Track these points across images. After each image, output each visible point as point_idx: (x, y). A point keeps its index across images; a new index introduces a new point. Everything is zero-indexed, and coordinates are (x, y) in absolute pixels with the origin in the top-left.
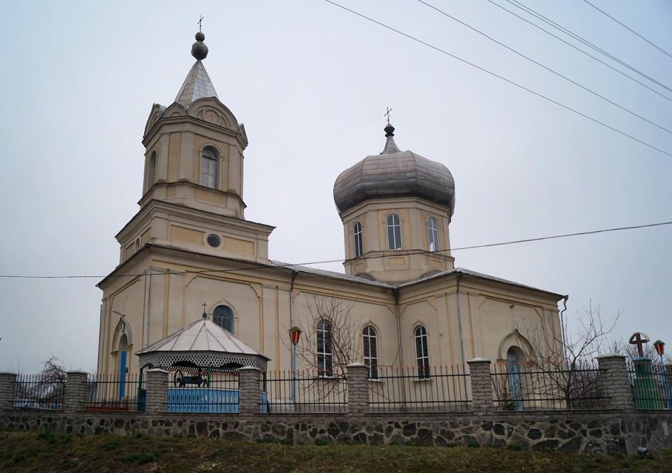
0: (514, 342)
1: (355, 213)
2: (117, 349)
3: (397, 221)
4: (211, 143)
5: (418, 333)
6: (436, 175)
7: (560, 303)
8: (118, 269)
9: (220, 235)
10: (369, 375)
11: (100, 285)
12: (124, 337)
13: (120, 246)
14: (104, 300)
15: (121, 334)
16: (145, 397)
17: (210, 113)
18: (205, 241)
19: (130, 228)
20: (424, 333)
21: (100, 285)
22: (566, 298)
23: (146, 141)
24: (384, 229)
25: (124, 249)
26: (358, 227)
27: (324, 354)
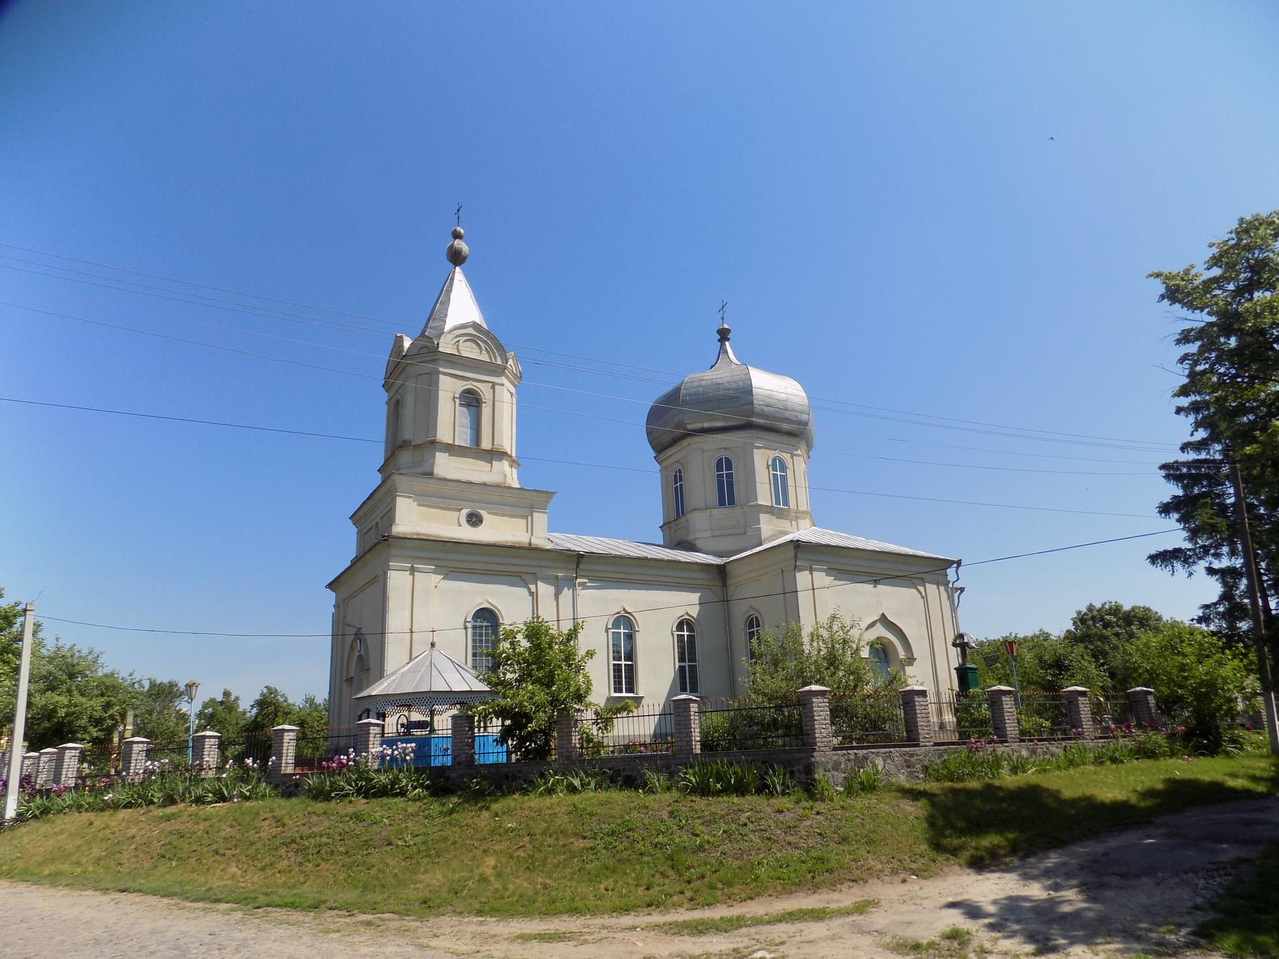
0: (880, 631)
1: (676, 453)
2: (352, 674)
3: (729, 466)
4: (469, 385)
5: (751, 626)
6: (783, 396)
7: (951, 572)
8: (355, 562)
9: (483, 513)
10: (377, 725)
11: (330, 586)
12: (361, 658)
13: (356, 530)
14: (337, 606)
15: (357, 654)
16: (831, 711)
17: (468, 344)
18: (463, 520)
19: (360, 514)
20: (758, 625)
21: (330, 586)
22: (959, 563)
23: (387, 386)
24: (712, 474)
25: (362, 535)
26: (678, 477)
27: (623, 663)
